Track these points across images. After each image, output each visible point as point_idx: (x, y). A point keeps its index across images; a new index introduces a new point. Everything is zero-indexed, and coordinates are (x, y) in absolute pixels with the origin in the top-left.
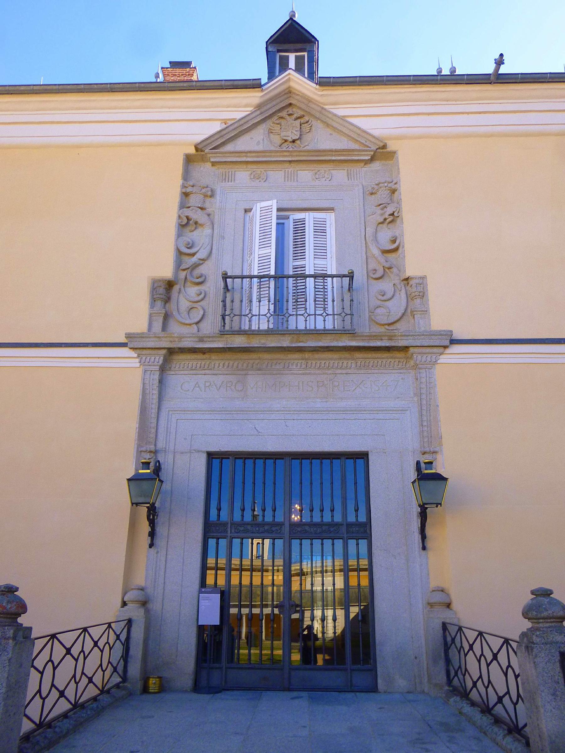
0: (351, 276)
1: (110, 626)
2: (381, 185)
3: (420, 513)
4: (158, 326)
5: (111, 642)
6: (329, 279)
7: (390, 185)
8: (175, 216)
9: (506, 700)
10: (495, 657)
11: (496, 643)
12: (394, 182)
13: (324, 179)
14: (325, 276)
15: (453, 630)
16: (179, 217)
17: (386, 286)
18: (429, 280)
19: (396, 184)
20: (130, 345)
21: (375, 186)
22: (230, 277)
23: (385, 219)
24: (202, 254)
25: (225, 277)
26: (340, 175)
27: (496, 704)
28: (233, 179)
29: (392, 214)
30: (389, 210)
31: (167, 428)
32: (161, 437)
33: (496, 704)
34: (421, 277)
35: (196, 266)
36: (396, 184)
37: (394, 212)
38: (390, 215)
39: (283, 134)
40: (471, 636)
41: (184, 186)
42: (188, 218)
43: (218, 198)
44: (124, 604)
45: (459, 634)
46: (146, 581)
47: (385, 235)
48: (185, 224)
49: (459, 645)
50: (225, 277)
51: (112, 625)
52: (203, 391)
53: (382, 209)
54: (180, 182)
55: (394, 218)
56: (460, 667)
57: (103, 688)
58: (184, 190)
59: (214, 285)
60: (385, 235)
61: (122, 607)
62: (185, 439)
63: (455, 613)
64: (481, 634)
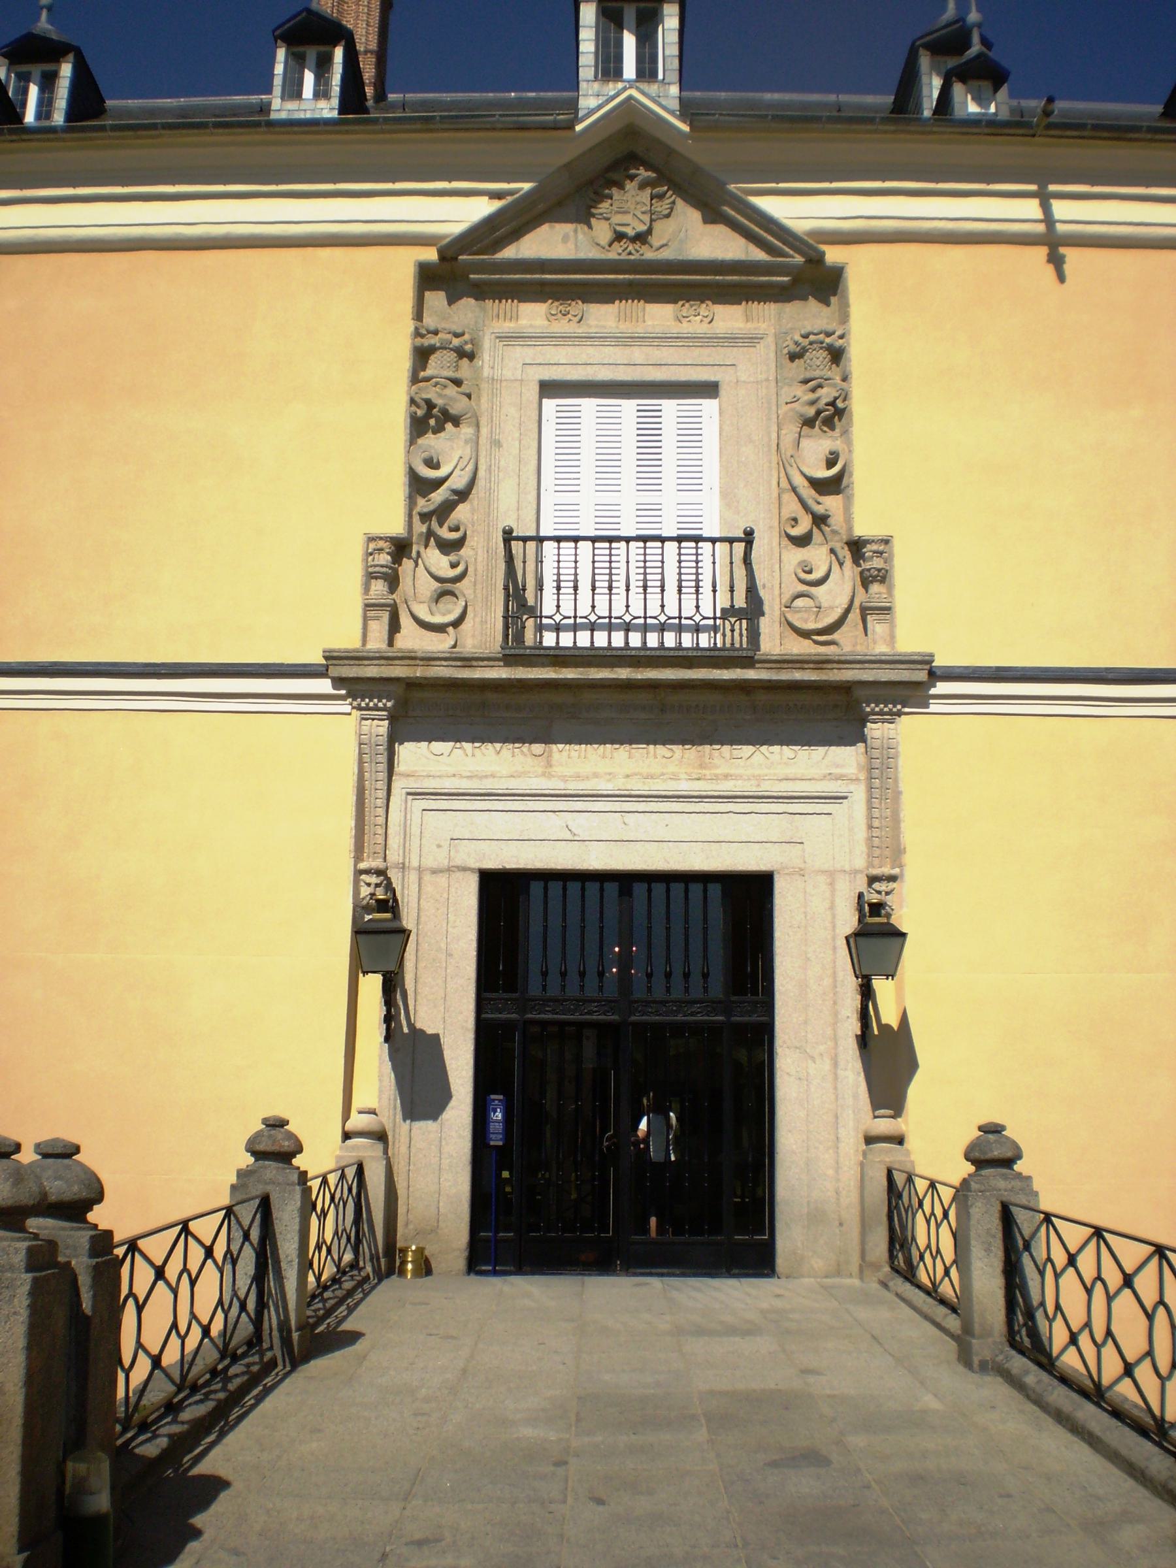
0: (748, 538)
1: (185, 1229)
2: (812, 338)
3: (861, 986)
4: (379, 628)
5: (194, 1267)
6: (706, 547)
7: (828, 340)
8: (404, 400)
9: (1084, 1340)
10: (1072, 1260)
11: (1131, 1254)
12: (837, 334)
13: (699, 318)
14: (697, 539)
15: (900, 1179)
16: (412, 401)
17: (818, 556)
18: (898, 547)
19: (841, 337)
20: (333, 671)
21: (801, 340)
22: (518, 539)
23: (818, 413)
24: (458, 481)
25: (508, 536)
26: (729, 318)
27: (1118, 1381)
28: (514, 315)
29: (832, 404)
30: (826, 394)
31: (405, 826)
32: (394, 842)
33: (1118, 1381)
34: (882, 540)
35: (446, 509)
36: (841, 337)
37: (836, 399)
38: (827, 405)
39: (617, 219)
40: (921, 1185)
41: (417, 334)
42: (430, 405)
43: (486, 357)
44: (347, 1136)
45: (1043, 1229)
46: (380, 1098)
47: (813, 454)
48: (426, 419)
49: (928, 1213)
50: (508, 536)
51: (141, 1243)
52: (470, 754)
53: (813, 390)
54: (409, 326)
55: (832, 416)
56: (929, 1246)
57: (184, 1377)
58: (419, 341)
59: (483, 554)
60: (813, 454)
61: (344, 1142)
62: (439, 846)
63: (908, 1153)
64: (1098, 1233)
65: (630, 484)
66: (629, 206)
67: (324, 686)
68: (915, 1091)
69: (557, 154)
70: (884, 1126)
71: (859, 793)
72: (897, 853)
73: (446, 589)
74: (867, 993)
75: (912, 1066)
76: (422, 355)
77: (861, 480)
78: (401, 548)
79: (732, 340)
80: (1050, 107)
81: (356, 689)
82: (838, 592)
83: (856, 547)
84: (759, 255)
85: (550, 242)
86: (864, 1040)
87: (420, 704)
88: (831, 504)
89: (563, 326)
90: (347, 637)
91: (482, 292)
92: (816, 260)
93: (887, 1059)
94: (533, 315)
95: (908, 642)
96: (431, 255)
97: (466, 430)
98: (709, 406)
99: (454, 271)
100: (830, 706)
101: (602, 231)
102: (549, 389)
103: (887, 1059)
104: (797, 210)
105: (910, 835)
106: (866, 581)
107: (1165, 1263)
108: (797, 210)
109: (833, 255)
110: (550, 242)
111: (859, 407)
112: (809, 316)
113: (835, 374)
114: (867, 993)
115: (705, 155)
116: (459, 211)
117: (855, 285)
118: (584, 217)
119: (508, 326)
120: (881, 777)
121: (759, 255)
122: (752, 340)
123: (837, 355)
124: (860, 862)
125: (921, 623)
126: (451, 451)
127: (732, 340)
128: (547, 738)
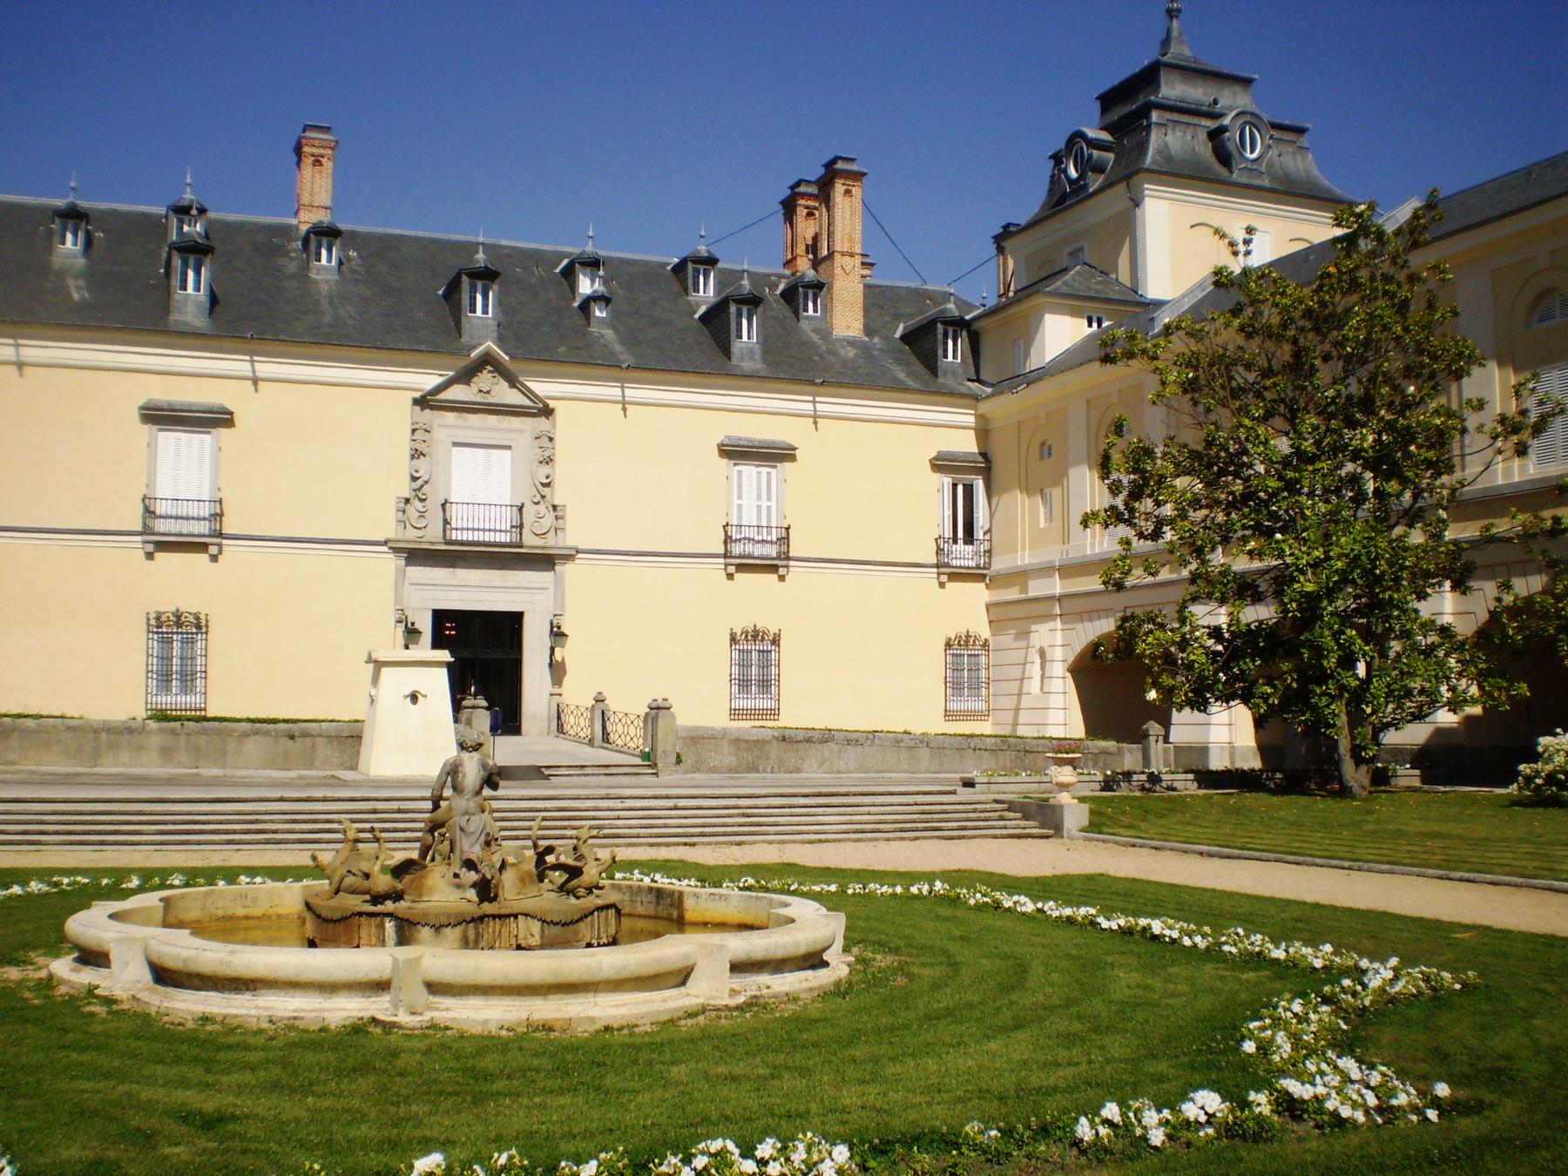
17: (542, 508)
26: (516, 422)
30: (547, 454)
48: (417, 454)
55: (549, 461)
65: (481, 484)
66: (485, 379)
67: (385, 549)
68: (566, 680)
69: (462, 363)
70: (556, 690)
71: (552, 588)
72: (563, 607)
73: (422, 515)
74: (552, 650)
75: (565, 672)
76: (414, 431)
77: (557, 484)
78: (407, 501)
79: (516, 431)
80: (884, 1061)
81: (396, 550)
82: (548, 521)
83: (555, 507)
84: (528, 403)
85: (457, 393)
86: (551, 665)
87: (417, 556)
88: (546, 491)
89: (461, 422)
90: (391, 535)
91: (433, 408)
92: (546, 406)
93: (557, 670)
94: (450, 417)
95: (570, 542)
96: (417, 395)
97: (427, 459)
98: (507, 453)
99: (424, 402)
100: (545, 561)
101: (474, 388)
102: (456, 444)
103: (557, 670)
104: (542, 387)
105: (568, 602)
106: (557, 518)
107: (443, 396)
108: (542, 387)
109: (552, 404)
110: (457, 393)
111: (557, 459)
112: (541, 423)
113: (550, 445)
114: (552, 650)
115: (513, 367)
116: (428, 380)
117: (558, 413)
118: (468, 383)
119: (441, 421)
120: (559, 583)
121: (528, 403)
122: (523, 431)
123: (551, 439)
124: (551, 609)
125: (572, 537)
126: (423, 466)
127: (516, 431)
128: (454, 566)
